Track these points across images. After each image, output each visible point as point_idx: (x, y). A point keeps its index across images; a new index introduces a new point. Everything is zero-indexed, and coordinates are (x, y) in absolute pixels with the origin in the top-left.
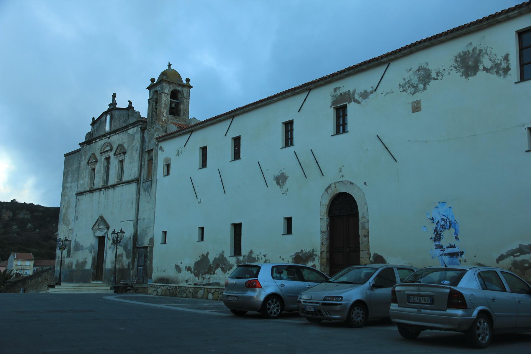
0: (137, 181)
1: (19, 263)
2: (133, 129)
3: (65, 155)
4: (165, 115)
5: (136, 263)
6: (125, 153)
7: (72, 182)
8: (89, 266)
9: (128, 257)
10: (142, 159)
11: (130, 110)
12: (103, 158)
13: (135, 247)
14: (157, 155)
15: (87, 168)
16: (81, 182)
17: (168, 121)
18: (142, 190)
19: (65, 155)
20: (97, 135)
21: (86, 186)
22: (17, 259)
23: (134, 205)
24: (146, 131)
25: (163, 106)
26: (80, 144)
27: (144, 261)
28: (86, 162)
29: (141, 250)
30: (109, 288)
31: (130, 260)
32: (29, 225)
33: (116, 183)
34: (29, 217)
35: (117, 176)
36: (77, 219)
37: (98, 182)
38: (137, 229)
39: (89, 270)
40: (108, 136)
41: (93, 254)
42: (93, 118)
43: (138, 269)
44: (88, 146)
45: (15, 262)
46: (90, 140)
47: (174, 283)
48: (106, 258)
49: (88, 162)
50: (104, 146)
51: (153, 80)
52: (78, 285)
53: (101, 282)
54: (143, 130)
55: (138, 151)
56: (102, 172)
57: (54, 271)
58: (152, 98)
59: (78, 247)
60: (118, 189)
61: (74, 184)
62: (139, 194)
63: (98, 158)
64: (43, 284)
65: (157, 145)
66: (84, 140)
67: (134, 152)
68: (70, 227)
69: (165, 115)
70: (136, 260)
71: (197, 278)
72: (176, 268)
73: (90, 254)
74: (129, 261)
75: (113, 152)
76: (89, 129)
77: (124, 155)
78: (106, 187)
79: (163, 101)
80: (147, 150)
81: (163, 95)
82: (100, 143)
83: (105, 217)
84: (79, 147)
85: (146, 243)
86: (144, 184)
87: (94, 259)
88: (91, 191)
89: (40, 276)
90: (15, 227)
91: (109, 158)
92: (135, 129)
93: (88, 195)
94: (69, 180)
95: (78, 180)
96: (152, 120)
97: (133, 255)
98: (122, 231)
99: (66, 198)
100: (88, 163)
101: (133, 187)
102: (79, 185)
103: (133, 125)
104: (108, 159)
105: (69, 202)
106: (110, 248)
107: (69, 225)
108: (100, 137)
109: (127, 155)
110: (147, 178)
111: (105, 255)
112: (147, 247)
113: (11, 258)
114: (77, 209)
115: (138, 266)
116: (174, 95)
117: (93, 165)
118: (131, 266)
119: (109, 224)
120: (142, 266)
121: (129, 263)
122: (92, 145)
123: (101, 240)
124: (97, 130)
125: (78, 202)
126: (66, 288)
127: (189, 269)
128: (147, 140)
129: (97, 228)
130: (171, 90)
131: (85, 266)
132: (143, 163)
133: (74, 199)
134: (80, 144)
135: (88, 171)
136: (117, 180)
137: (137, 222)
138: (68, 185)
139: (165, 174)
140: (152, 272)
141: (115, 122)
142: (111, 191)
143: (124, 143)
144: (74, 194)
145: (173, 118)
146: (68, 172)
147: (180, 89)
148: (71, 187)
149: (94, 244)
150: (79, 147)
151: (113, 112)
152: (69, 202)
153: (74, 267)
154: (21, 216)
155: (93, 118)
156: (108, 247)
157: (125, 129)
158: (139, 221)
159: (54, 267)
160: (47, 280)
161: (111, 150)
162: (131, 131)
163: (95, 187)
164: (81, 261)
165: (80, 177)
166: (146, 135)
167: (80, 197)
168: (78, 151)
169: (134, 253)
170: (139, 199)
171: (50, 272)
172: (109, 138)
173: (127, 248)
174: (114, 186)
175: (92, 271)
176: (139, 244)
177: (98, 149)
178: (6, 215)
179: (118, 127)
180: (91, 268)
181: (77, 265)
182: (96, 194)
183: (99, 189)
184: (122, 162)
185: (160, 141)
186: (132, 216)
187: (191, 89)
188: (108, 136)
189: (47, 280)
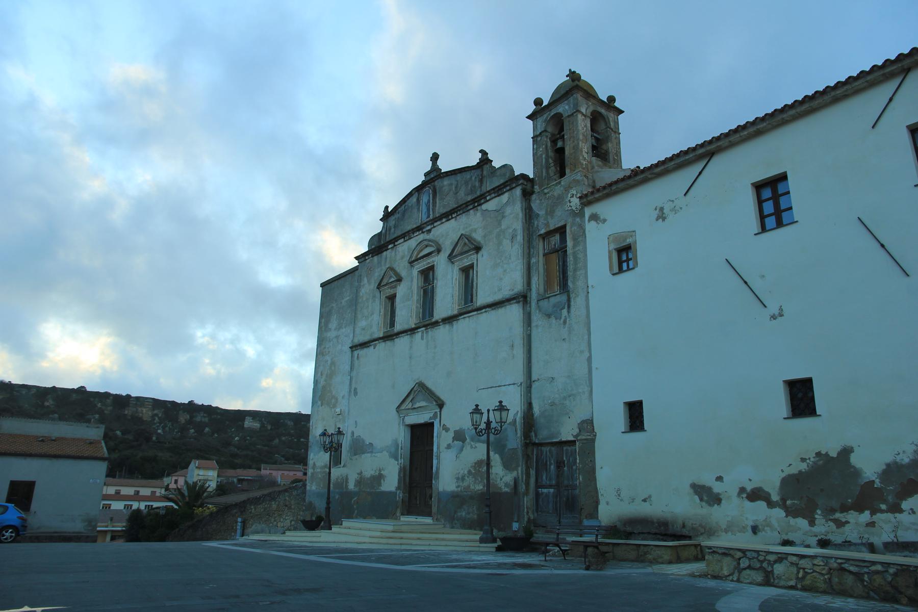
0: (522, 298)
1: (201, 472)
2: (497, 199)
3: (323, 285)
4: (586, 156)
5: (532, 480)
6: (478, 249)
7: (339, 327)
8: (391, 483)
9: (508, 465)
10: (529, 253)
11: (486, 167)
12: (415, 272)
13: (529, 443)
14: (581, 235)
15: (374, 297)
16: (362, 323)
18: (536, 318)
19: (323, 285)
20: (399, 233)
21: (375, 329)
22: (198, 468)
23: (519, 352)
24: (534, 197)
25: (581, 137)
26: (357, 258)
27: (558, 476)
29: (545, 449)
30: (477, 537)
31: (519, 472)
32: (207, 429)
33: (456, 312)
34: (206, 420)
36: (356, 393)
38: (530, 405)
39: (390, 493)
40: (429, 228)
41: (401, 461)
42: (387, 207)
43: (537, 495)
44: (376, 258)
45: (197, 472)
47: (690, 538)
48: (438, 469)
49: (379, 284)
50: (418, 248)
51: (538, 102)
52: (390, 528)
53: (428, 520)
54: (527, 195)
55: (520, 238)
56: (415, 297)
57: (304, 492)
59: (360, 448)
60: (463, 324)
61: (348, 330)
63: (403, 273)
64: (280, 515)
65: (581, 214)
67: (506, 242)
68: (338, 410)
69: (586, 156)
70: (533, 472)
71: (802, 523)
72: (696, 492)
73: (393, 461)
74: (515, 474)
75: (444, 256)
76: (378, 227)
77: (477, 253)
79: (580, 128)
80: (543, 231)
81: (580, 116)
82: (405, 248)
83: (429, 384)
84: (356, 263)
85: (568, 431)
86: (544, 303)
87: (402, 470)
88: (389, 337)
89: (274, 499)
90: (192, 431)
91: (432, 268)
92: (505, 197)
93: (381, 346)
94: (333, 324)
95: (354, 321)
97: (526, 463)
98: (340, 432)
99: (328, 358)
101: (514, 312)
102: (358, 331)
103: (498, 191)
104: (428, 274)
105: (333, 363)
106: (449, 447)
107: (335, 406)
108: (406, 236)
109: (483, 252)
110: (546, 291)
111: (435, 462)
112: (572, 443)
113: (192, 466)
114: (354, 373)
115: (538, 486)
116: (595, 118)
117: (392, 288)
118: (522, 488)
119: (442, 398)
120: (550, 486)
121: (516, 481)
122: (385, 253)
123: (422, 435)
125: (356, 362)
126: (355, 534)
127: (756, 495)
128: (542, 213)
129: (410, 406)
130: (575, 121)
131: (380, 485)
133: (345, 358)
134: (357, 258)
136: (457, 307)
137: (529, 387)
138: (332, 334)
139: (616, 269)
140: (597, 503)
141: (442, 199)
143: (475, 230)
144: (346, 348)
145: (600, 163)
147: (603, 111)
148: (337, 337)
150: (356, 263)
151: (438, 183)
152: (333, 363)
153: (351, 486)
154: (198, 419)
155: (387, 207)
156: (443, 445)
157: (477, 201)
158: (535, 386)
159: (305, 485)
160: (290, 508)
161: (439, 251)
162: (491, 205)
163: (398, 327)
164: (369, 473)
165: (359, 316)
166: (535, 205)
167: (362, 352)
169: (527, 457)
171: (295, 493)
172: (429, 231)
173: (504, 446)
174: (449, 320)
175: (400, 495)
176: (543, 435)
177: (402, 258)
178: (183, 418)
180: (398, 488)
181: (360, 482)
185: (590, 203)
186: (520, 377)
187: (621, 117)
188: (429, 228)
189: (290, 508)
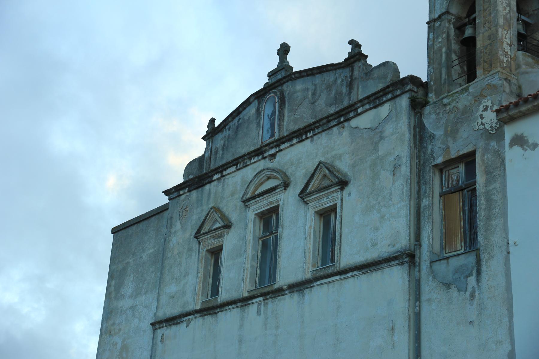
0: (408, 258)
3: (115, 231)
4: (507, 49)
6: (343, 184)
7: (137, 293)
10: (419, 192)
11: (358, 66)
12: (251, 215)
15: (190, 250)
16: (171, 288)
17: (518, 67)
18: (429, 288)
21: (189, 297)
24: (428, 109)
25: (501, 21)
26: (167, 192)
28: (190, 233)
35: (310, 255)
37: (236, 277)
42: (212, 121)
46: (199, 175)
49: (198, 232)
50: (257, 181)
54: (417, 106)
55: (405, 169)
56: (250, 252)
58: (447, 12)
60: (319, 294)
61: (148, 298)
62: (418, 298)
63: (234, 217)
66: (181, 180)
69: (507, 49)
76: (199, 148)
77: (342, 189)
78: (267, 290)
80: (439, 160)
82: (237, 180)
84: (165, 200)
88: (209, 310)
91: (275, 210)
94: (128, 289)
96: (449, 74)
99: (118, 339)
100: (198, 235)
101: (396, 278)
102: (164, 299)
103: (375, 100)
104: (269, 218)
110: (443, 248)
117: (215, 237)
122: (207, 187)
124: (224, 148)
132: (425, 202)
135: (195, 257)
136: (311, 269)
138: (125, 303)
142: (288, 304)
144: (146, 325)
145: (530, 60)
146: (124, 269)
148: (133, 308)
149: (226, 235)
150: (165, 200)
151: (287, 88)
155: (212, 121)
157: (344, 115)
161: (286, 185)
162: (365, 120)
163: (223, 296)
165: (167, 277)
167: (169, 331)
168: (163, 209)
170: (418, 315)
172: (273, 156)
174: (299, 287)
179: (308, 120)
182: (229, 318)
183: (243, 302)
184: (327, 215)
